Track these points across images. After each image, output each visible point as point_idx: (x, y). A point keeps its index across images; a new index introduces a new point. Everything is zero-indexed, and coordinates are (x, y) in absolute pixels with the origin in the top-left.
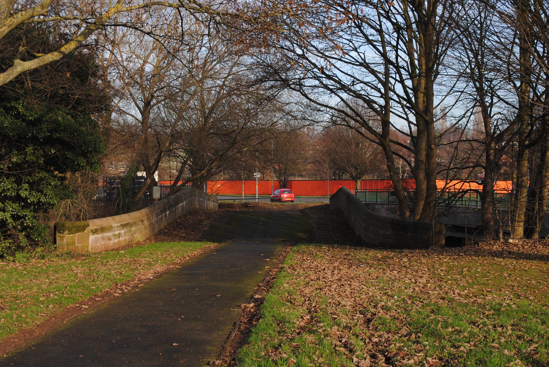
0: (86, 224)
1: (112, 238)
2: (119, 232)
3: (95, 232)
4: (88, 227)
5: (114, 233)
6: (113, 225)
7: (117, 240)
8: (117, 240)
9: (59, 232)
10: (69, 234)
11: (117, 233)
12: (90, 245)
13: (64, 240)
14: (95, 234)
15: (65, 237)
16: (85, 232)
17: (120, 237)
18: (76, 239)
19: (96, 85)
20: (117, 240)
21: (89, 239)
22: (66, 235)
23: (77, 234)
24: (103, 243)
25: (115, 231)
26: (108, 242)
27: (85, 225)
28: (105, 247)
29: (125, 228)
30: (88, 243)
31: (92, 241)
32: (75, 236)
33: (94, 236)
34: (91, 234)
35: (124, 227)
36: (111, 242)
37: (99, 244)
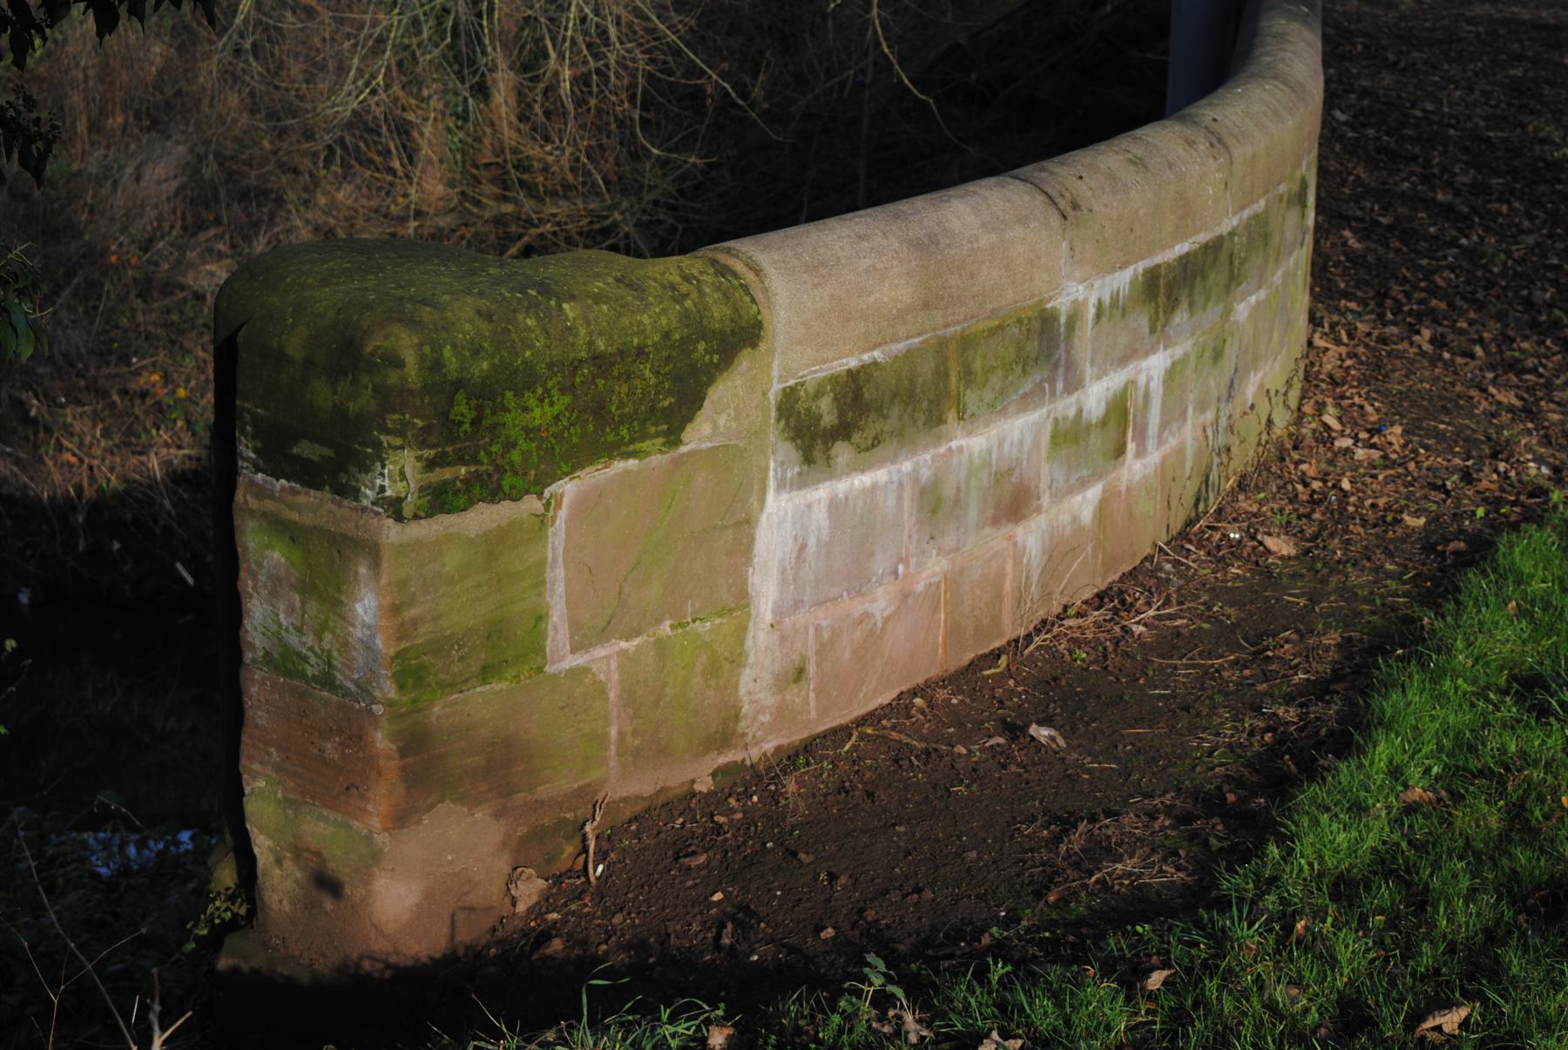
0: (719, 313)
1: (1046, 473)
2: (1115, 380)
3: (842, 431)
4: (744, 361)
5: (1066, 406)
6: (1061, 304)
7: (1094, 493)
8: (1094, 493)
9: (277, 460)
10: (440, 500)
11: (1095, 396)
12: (760, 638)
13: (366, 607)
14: (842, 452)
15: (373, 553)
16: (699, 434)
17: (1120, 451)
18: (557, 577)
19: (518, 394)
20: (1085, 503)
21: (743, 548)
22: (392, 533)
23: (567, 488)
24: (936, 567)
25: (1074, 384)
26: (996, 539)
27: (696, 326)
28: (954, 630)
29: (1180, 317)
30: (742, 600)
31: (791, 576)
32: (543, 520)
33: (821, 493)
34: (780, 457)
35: (1173, 305)
36: (1031, 536)
37: (880, 603)
